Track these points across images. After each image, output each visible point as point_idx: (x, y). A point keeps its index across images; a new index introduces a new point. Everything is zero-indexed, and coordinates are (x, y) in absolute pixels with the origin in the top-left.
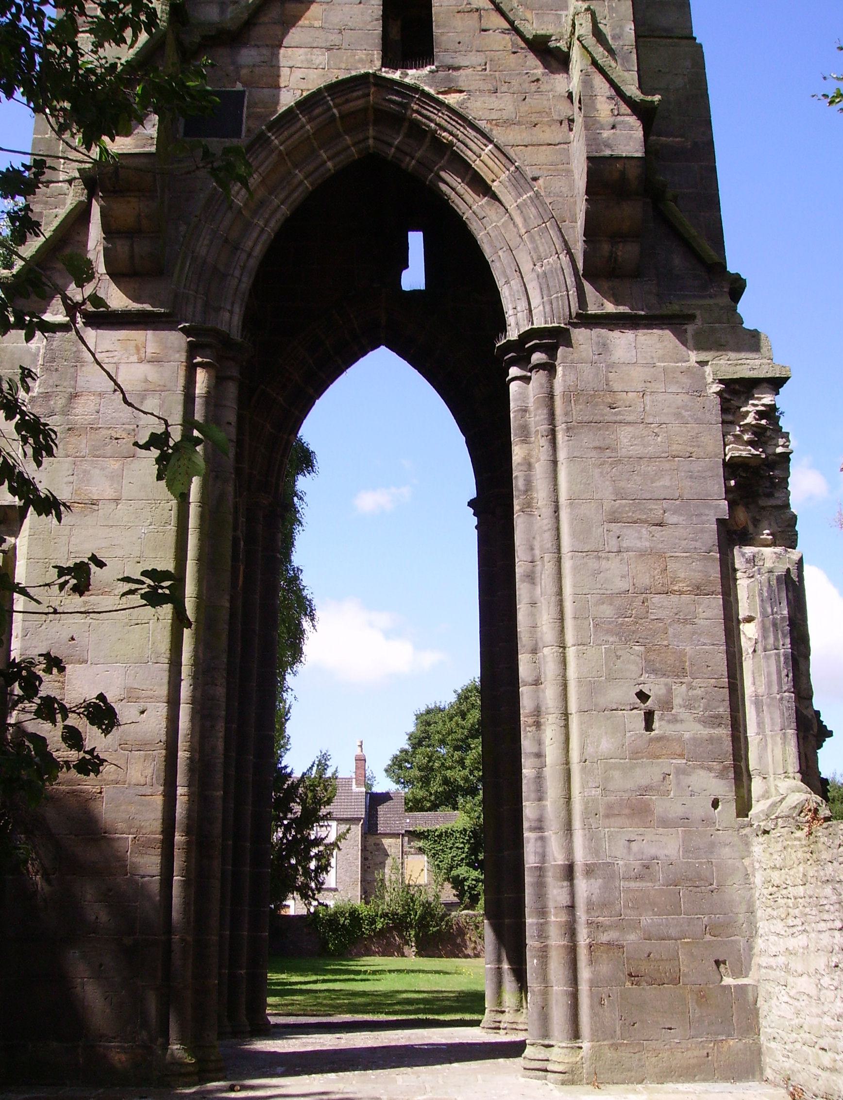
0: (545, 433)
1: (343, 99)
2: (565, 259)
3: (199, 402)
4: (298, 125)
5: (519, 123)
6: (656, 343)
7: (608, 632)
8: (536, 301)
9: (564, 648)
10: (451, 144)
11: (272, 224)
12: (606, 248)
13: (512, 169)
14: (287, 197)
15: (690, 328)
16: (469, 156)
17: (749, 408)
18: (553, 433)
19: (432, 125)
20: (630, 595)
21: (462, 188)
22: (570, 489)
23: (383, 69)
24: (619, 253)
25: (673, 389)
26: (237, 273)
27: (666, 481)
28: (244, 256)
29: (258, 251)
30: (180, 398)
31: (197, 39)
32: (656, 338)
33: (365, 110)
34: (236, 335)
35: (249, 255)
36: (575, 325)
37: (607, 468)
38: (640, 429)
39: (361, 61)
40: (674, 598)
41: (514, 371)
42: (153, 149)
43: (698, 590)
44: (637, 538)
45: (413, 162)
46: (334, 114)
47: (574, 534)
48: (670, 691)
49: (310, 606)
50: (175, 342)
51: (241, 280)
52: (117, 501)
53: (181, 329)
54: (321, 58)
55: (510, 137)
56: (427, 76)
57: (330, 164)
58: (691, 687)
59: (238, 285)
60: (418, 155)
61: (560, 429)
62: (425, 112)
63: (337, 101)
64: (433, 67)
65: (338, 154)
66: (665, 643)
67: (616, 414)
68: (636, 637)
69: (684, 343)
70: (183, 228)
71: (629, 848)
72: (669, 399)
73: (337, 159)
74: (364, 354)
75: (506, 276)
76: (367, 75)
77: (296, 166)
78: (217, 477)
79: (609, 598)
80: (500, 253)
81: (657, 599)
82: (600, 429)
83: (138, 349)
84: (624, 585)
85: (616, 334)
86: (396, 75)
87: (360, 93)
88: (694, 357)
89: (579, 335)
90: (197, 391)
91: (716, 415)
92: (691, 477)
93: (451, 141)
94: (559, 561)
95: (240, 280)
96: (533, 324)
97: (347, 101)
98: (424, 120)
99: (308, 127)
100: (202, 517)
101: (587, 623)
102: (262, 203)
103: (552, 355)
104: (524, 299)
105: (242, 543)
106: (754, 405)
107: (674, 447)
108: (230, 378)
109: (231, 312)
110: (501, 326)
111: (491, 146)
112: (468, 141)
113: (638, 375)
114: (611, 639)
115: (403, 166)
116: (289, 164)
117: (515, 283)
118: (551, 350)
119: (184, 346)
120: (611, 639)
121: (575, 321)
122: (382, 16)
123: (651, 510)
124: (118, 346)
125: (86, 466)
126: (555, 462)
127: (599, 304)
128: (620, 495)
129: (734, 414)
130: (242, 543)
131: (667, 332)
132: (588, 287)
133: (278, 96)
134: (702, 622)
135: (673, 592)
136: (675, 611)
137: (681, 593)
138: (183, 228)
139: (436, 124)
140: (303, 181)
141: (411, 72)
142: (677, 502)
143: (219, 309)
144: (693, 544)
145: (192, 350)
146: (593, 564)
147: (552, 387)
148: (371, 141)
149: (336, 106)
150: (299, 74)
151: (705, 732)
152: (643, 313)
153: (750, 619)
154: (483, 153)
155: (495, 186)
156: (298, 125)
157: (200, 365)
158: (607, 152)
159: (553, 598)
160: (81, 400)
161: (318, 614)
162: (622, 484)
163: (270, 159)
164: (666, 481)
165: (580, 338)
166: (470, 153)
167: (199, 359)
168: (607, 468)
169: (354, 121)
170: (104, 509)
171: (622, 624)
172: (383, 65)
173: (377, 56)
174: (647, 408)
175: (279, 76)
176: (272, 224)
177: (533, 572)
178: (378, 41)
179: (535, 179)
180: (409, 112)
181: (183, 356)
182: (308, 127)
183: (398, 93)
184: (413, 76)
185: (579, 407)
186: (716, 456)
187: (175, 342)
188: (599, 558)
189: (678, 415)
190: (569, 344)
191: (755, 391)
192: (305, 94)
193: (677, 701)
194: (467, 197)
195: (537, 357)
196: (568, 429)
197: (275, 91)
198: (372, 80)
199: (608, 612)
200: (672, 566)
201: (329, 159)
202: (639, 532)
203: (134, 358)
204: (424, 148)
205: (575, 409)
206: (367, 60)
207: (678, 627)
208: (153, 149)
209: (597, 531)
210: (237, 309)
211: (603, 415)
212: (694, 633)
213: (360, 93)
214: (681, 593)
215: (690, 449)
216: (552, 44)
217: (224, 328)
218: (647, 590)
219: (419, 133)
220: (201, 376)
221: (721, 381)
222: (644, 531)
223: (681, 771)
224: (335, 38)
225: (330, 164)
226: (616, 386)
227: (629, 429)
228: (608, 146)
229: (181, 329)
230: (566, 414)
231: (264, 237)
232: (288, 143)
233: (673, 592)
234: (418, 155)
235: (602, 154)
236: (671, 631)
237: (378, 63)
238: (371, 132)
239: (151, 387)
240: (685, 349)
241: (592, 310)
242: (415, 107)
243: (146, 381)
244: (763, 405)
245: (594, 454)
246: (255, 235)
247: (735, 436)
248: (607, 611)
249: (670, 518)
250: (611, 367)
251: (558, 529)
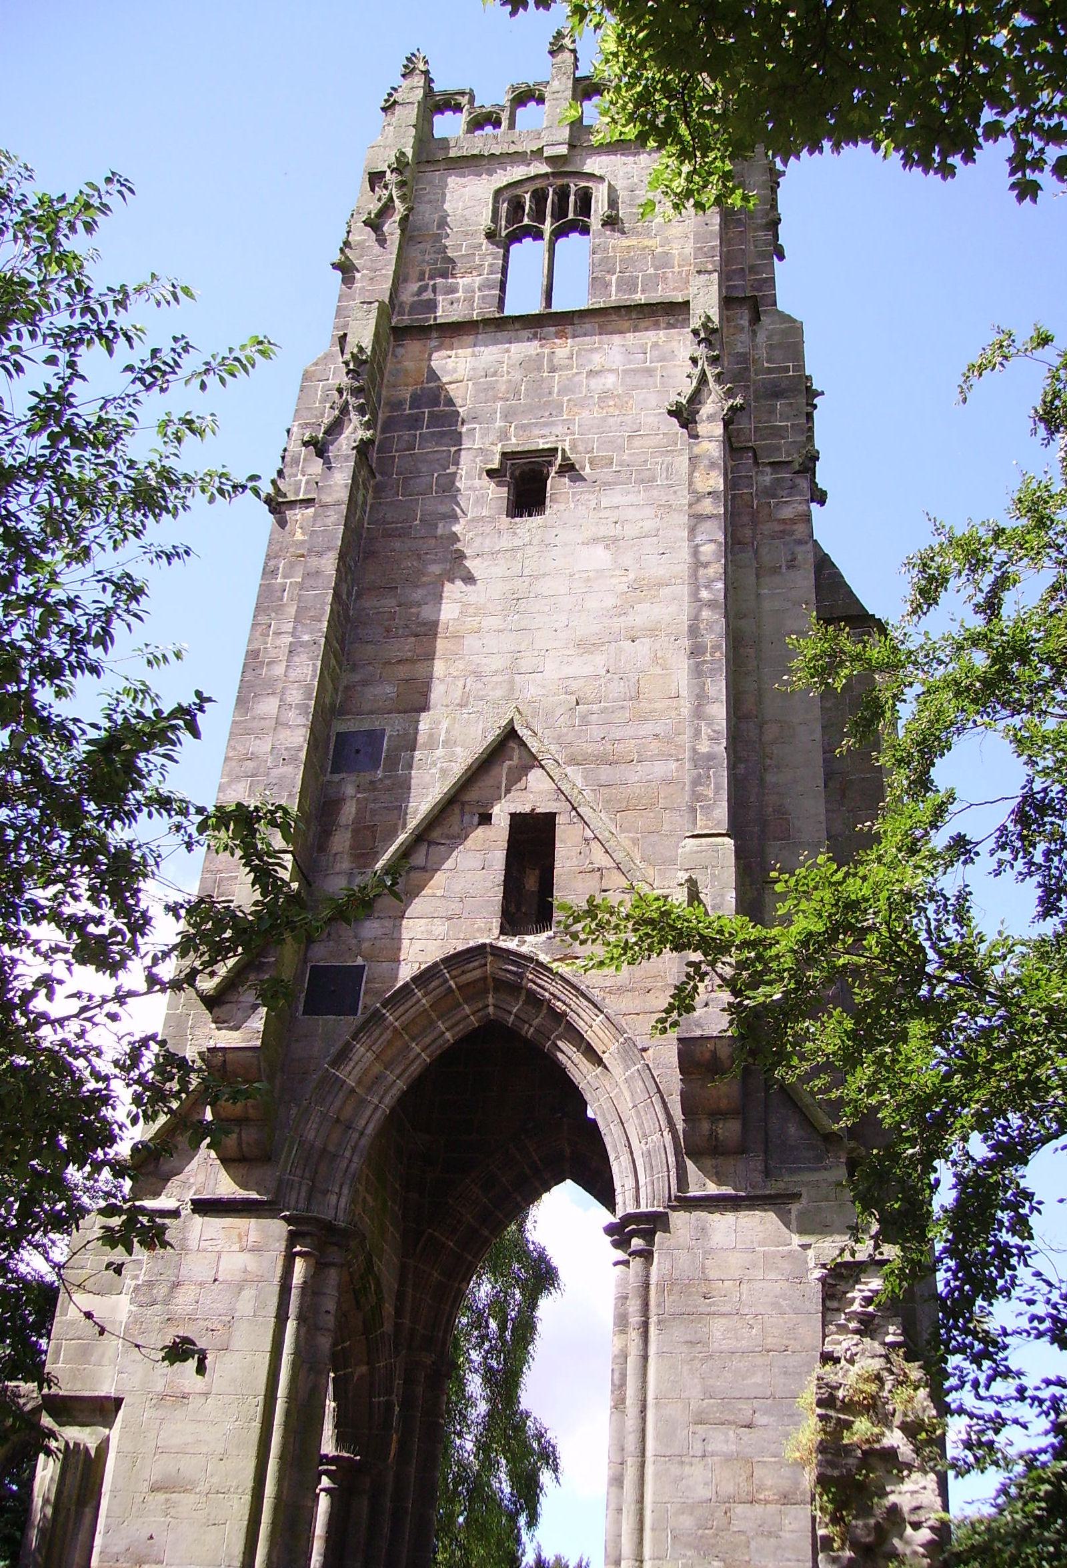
0: (637, 1326)
1: (460, 971)
2: (668, 1137)
3: (295, 1294)
4: (414, 1000)
5: (632, 990)
6: (756, 1227)
7: (688, 1545)
8: (642, 1181)
9: (642, 1562)
10: (564, 1014)
11: (387, 1100)
12: (705, 1126)
13: (622, 1040)
14: (404, 1071)
15: (795, 1208)
16: (581, 1025)
17: (856, 1294)
18: (646, 1325)
19: (547, 994)
20: (712, 1504)
21: (578, 1057)
22: (657, 1387)
23: (502, 937)
24: (720, 1131)
25: (772, 1276)
26: (348, 1154)
27: (758, 1379)
28: (356, 1135)
29: (370, 1130)
30: (275, 1289)
32: (758, 1220)
33: (484, 979)
35: (362, 1134)
36: (674, 1208)
37: (697, 1363)
39: (479, 930)
40: (758, 1508)
42: (258, 1043)
44: (723, 1441)
45: (532, 1029)
46: (450, 986)
47: (657, 1437)
49: (553, 1452)
50: (276, 1229)
51: (353, 1160)
52: (206, 1395)
53: (284, 1218)
54: (440, 928)
55: (623, 1005)
56: (544, 942)
57: (448, 1035)
59: (348, 1166)
60: (535, 1022)
61: (653, 1320)
62: (539, 981)
63: (454, 973)
64: (551, 933)
65: (457, 1024)
66: (747, 1558)
67: (710, 1305)
68: (715, 1552)
69: (787, 1225)
70: (294, 1112)
72: (769, 1286)
73: (457, 1029)
75: (617, 1151)
76: (484, 946)
77: (413, 1039)
78: (311, 1369)
79: (688, 1508)
80: (612, 1126)
81: (739, 1509)
82: (692, 1321)
83: (240, 1236)
84: (706, 1493)
85: (717, 1216)
86: (511, 943)
87: (476, 964)
88: (796, 1240)
89: (678, 1219)
90: (295, 1281)
91: (817, 1304)
92: (785, 1373)
93: (564, 1011)
94: (642, 1466)
95: (350, 1161)
96: (638, 1206)
97: (463, 972)
98: (539, 990)
99: (424, 1001)
100: (288, 1413)
101: (664, 1535)
102: (378, 1078)
103: (650, 1241)
104: (632, 1176)
105: (397, 1409)
106: (861, 1291)
107: (770, 1340)
108: (333, 1264)
109: (339, 1195)
111: (602, 1016)
112: (580, 1011)
113: (736, 1260)
114: (689, 1553)
115: (523, 1033)
116: (407, 1038)
117: (625, 1159)
118: (649, 1236)
119: (285, 1234)
120: (689, 1553)
121: (675, 1203)
122: (505, 881)
123: (740, 1410)
124: (222, 1234)
126: (645, 1358)
127: (702, 1185)
128: (708, 1394)
129: (840, 1300)
130: (397, 1409)
131: (771, 1214)
132: (690, 1165)
133: (398, 969)
134: (788, 1535)
135: (758, 1501)
136: (759, 1522)
137: (767, 1502)
139: (551, 994)
140: (420, 1054)
141: (528, 938)
142: (769, 1401)
143: (326, 1192)
145: (293, 1239)
146: (675, 1470)
147: (648, 1275)
148: (491, 1009)
149: (453, 978)
150: (418, 945)
152: (743, 1194)
154: (594, 1024)
155: (605, 1057)
156: (414, 1000)
157: (300, 1254)
158: (698, 1033)
159: (633, 1507)
161: (562, 1463)
162: (711, 1382)
163: (384, 1037)
164: (758, 1379)
165: (678, 1222)
166: (582, 1023)
167: (298, 1248)
168: (697, 1363)
169: (473, 991)
170: (195, 1403)
171: (701, 1537)
172: (502, 932)
173: (496, 923)
174: (743, 1298)
175: (399, 949)
176: (387, 1100)
177: (622, 1475)
178: (498, 908)
179: (645, 1050)
180: (525, 981)
181: (282, 1245)
182: (424, 1001)
183: (514, 963)
184: (531, 944)
185: (672, 1298)
186: (813, 1350)
187: (276, 1229)
188: (682, 1462)
189: (775, 1305)
190: (667, 1229)
191: (862, 1275)
192: (423, 967)
194: (581, 1066)
195: (637, 1243)
196: (659, 1322)
197: (394, 965)
198: (488, 949)
199: (687, 1523)
201: (448, 1029)
202: (726, 1434)
203: (236, 1247)
204: (542, 1015)
205: (668, 1299)
206: (484, 928)
207: (762, 1541)
208: (258, 1043)
209: (682, 1433)
211: (696, 1306)
212: (778, 1548)
213: (476, 964)
214: (767, 1502)
215: (786, 1342)
217: (328, 1215)
218: (731, 1499)
219: (535, 1001)
220: (299, 1265)
222: (731, 1433)
224: (455, 907)
225: (448, 1035)
226: (712, 1274)
227: (723, 1321)
228: (699, 1025)
229: (284, 1218)
230: (659, 1305)
231: (379, 1113)
232: (403, 1018)
233: (758, 1501)
234: (535, 1022)
235: (692, 1035)
236: (753, 1545)
237: (496, 932)
238: (491, 1000)
239: (249, 1277)
240: (787, 1231)
241: (694, 1191)
242: (531, 976)
243: (245, 1271)
244: (870, 1290)
245: (685, 1348)
246: (368, 1112)
247: (838, 1326)
248: (687, 1522)
249: (761, 1419)
250: (708, 1253)
251: (644, 1430)
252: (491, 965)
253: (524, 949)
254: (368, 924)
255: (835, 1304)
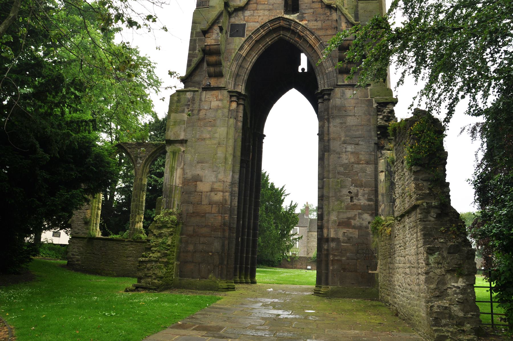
10: (303, 36)
11: (253, 60)
31: (233, 9)
34: (243, 93)
38: (353, 118)
40: (360, 166)
41: (320, 101)
43: (367, 163)
48: (358, 191)
54: (267, 13)
58: (364, 190)
71: (344, 234)
74: (288, 90)
76: (280, 17)
81: (355, 166)
86: (287, 16)
110: (317, 88)
125: (202, 129)
128: (346, 136)
135: (360, 164)
137: (363, 164)
138: (229, 64)
144: (367, 150)
150: (261, 18)
151: (367, 203)
153: (382, 172)
160: (202, 111)
173: (282, 11)
176: (253, 60)
184: (292, 17)
193: (360, 194)
200: (361, 156)
203: (215, 100)
210: (243, 85)
216: (332, 6)
217: (240, 91)
218: (353, 163)
221: (377, 103)
223: (360, 214)
224: (271, 7)
227: (350, 117)
237: (283, 13)
243: (218, 106)
249: (361, 143)
252: (282, 23)
253: (291, 18)
254: (246, 12)
255: (380, 113)
